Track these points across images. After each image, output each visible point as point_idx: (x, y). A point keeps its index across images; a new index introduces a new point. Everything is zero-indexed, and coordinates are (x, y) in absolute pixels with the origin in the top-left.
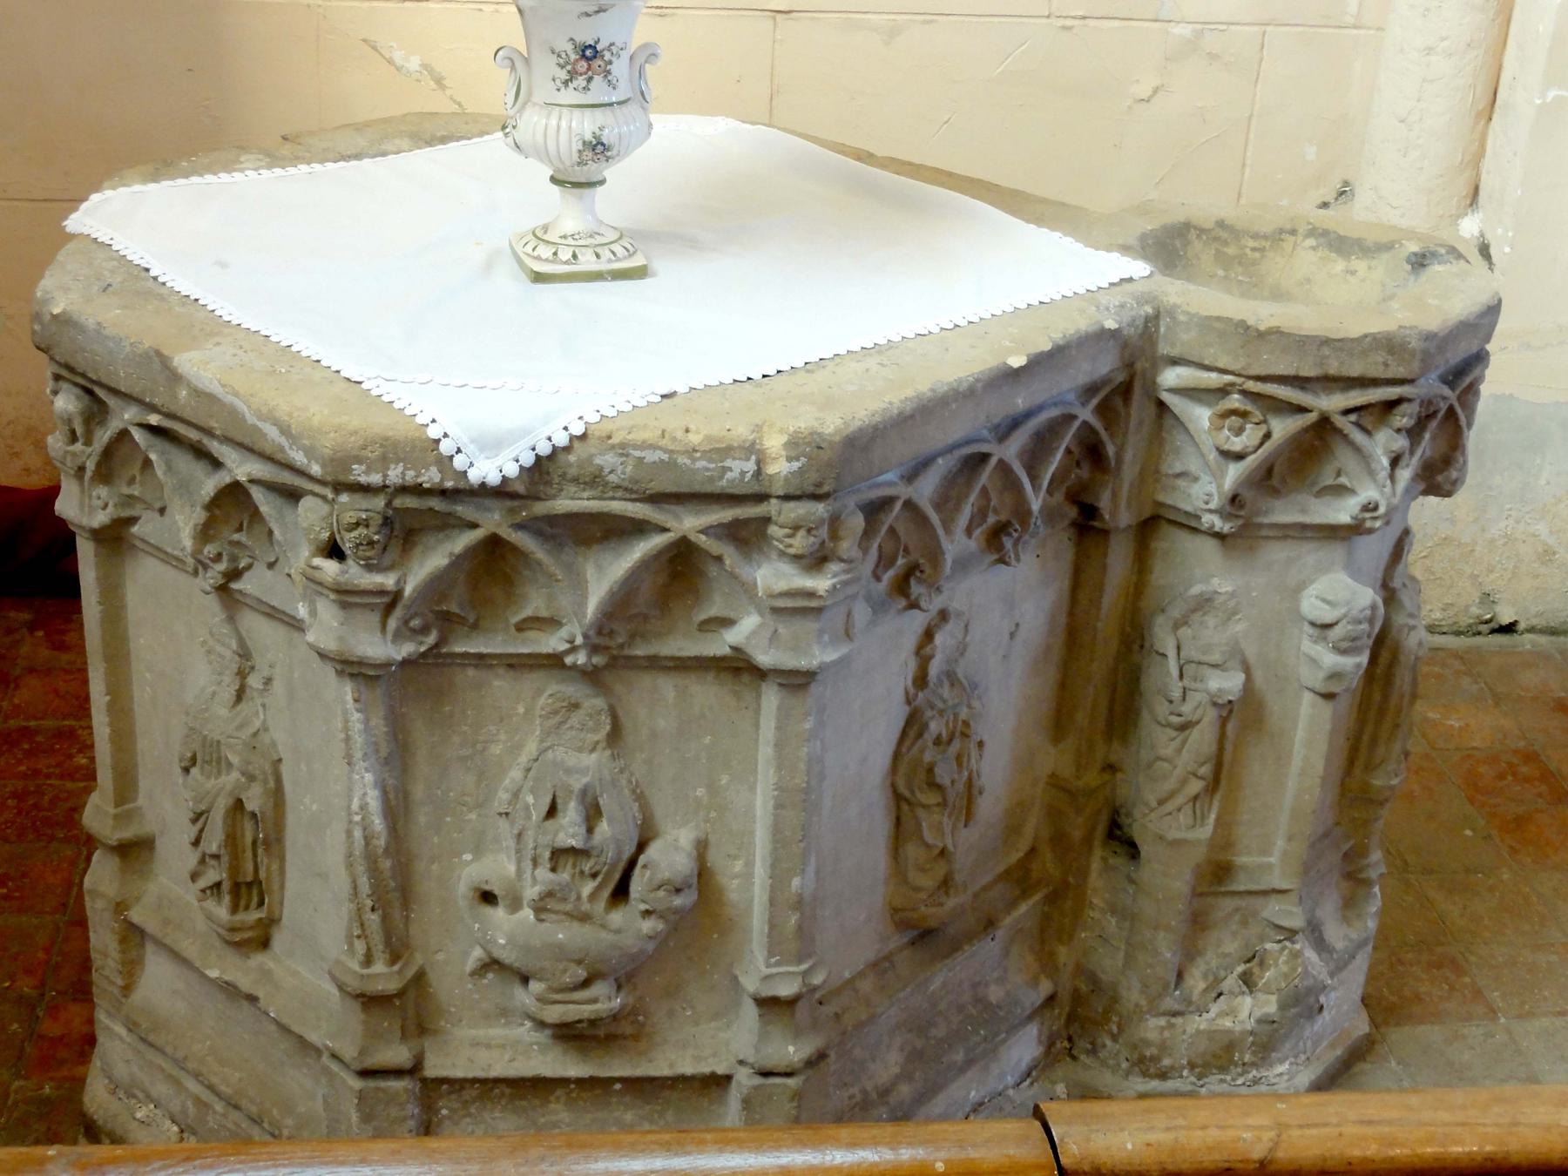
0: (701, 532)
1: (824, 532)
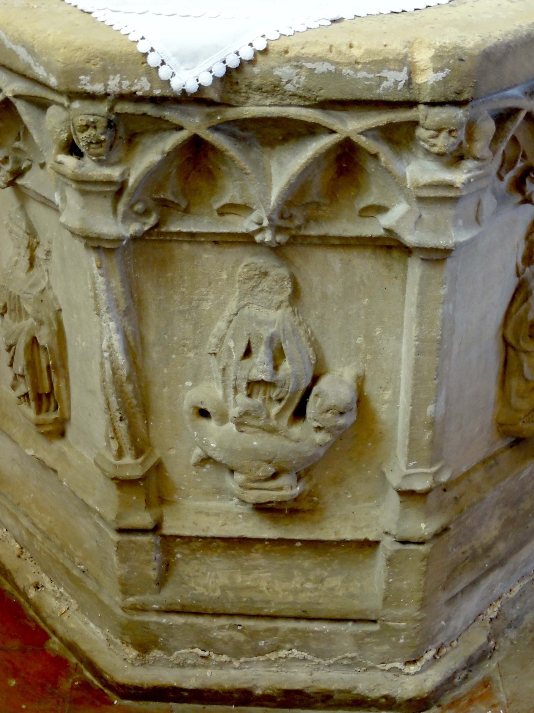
0: (361, 133)
1: (461, 134)
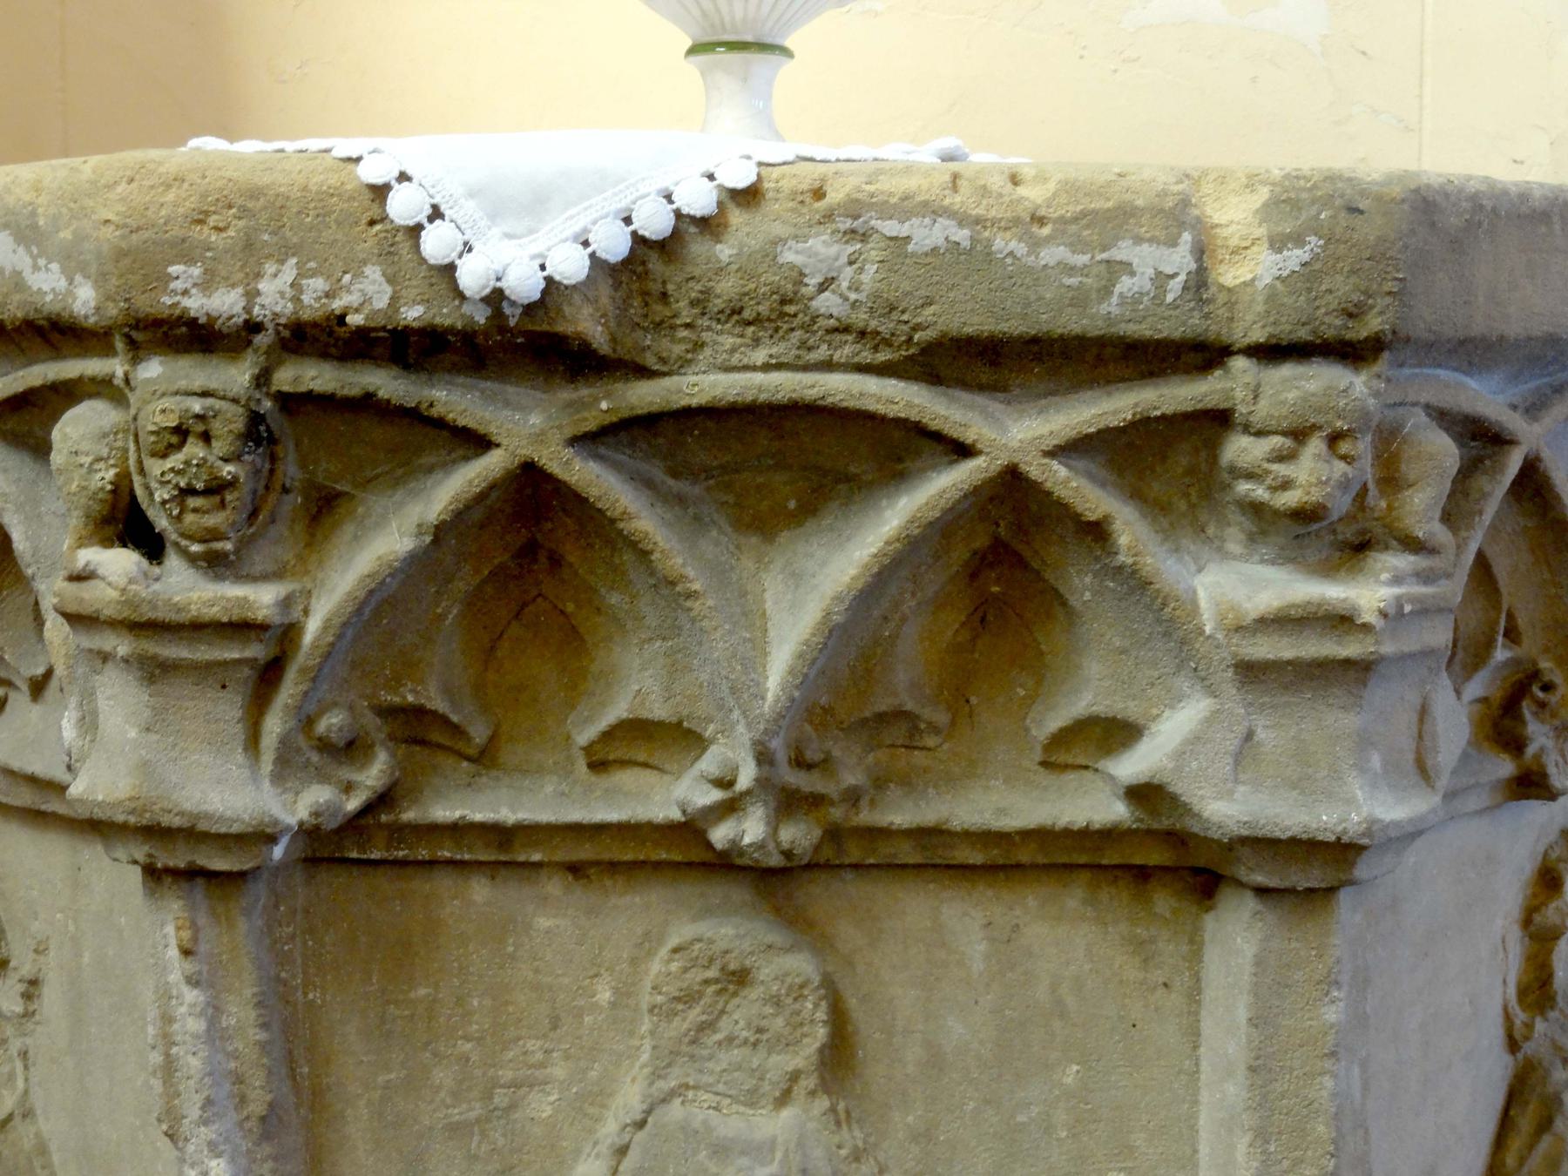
0: (1052, 453)
